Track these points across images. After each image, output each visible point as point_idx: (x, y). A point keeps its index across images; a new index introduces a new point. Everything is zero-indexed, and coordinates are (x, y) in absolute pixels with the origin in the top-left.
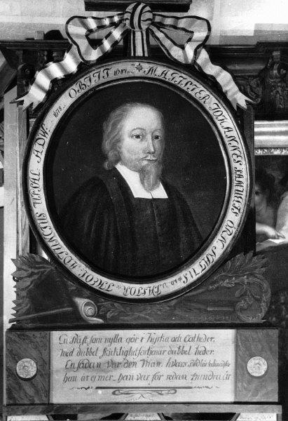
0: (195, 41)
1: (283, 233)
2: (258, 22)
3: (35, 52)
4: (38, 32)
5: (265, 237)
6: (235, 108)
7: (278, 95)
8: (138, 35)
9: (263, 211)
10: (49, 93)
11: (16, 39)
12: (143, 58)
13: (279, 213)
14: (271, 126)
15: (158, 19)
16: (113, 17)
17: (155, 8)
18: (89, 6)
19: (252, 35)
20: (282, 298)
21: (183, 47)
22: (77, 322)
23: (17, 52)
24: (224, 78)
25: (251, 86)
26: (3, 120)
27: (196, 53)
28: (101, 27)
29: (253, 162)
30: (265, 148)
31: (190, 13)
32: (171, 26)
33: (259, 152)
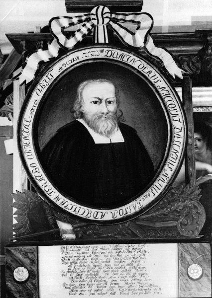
0: (144, 28)
5: (206, 172)
6: (174, 77)
10: (36, 74)
11: (21, 32)
12: (104, 45)
14: (208, 91)
17: (113, 10)
18: (70, 9)
19: (191, 25)
21: (133, 34)
22: (56, 239)
23: (22, 42)
25: (192, 62)
26: (13, 91)
27: (146, 41)
29: (191, 118)
30: (204, 107)
31: (142, 11)
33: (195, 110)
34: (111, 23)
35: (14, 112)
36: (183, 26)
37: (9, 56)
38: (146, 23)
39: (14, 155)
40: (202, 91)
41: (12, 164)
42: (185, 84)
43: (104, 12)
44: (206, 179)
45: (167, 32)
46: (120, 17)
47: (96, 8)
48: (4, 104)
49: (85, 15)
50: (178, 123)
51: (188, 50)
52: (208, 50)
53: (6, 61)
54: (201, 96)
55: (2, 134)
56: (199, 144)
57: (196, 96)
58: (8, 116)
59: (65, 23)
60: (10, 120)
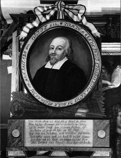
1: (114, 84)
4: (25, 11)
5: (107, 85)
7: (112, 34)
8: (61, 12)
10: (28, 34)
12: (62, 20)
13: (112, 77)
14: (109, 45)
15: (67, 6)
16: (49, 7)
17: (66, 3)
18: (42, 2)
19: (101, 12)
20: (113, 108)
24: (91, 26)
25: (102, 30)
28: (48, 9)
31: (78, 4)
35: (13, 53)
36: (97, 12)
37: (11, 25)
39: (12, 74)
42: (99, 41)
44: (107, 88)
45: (89, 15)
46: (70, 7)
48: (8, 49)
53: (9, 27)
54: (105, 47)
55: (6, 64)
57: (103, 47)
58: (9, 55)
60: (10, 56)
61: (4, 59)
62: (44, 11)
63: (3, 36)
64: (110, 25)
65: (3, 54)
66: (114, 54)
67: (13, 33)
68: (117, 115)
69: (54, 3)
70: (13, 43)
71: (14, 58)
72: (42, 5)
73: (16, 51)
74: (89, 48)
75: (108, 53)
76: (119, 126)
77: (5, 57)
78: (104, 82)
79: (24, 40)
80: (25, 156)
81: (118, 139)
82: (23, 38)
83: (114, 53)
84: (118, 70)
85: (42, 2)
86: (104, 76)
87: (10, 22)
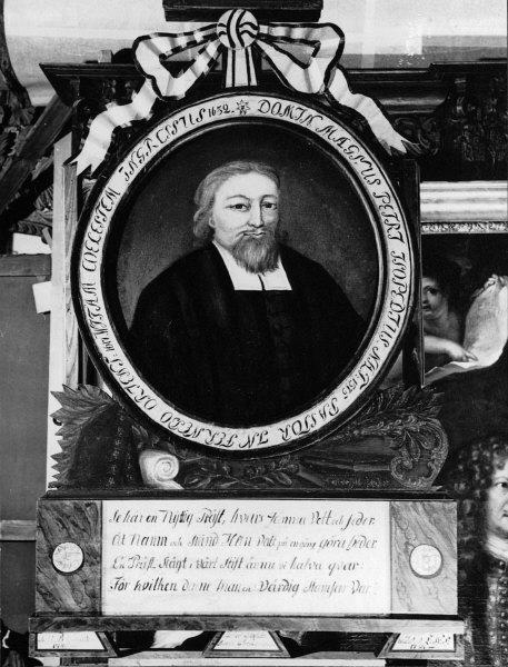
1: (474, 352)
2: (430, 33)
3: (100, 81)
5: (446, 358)
8: (240, 53)
9: (445, 317)
10: (112, 149)
11: (72, 62)
12: (247, 90)
13: (468, 321)
20: (474, 453)
21: (305, 66)
22: (139, 488)
24: (367, 107)
27: (328, 78)
31: (321, 21)
32: (283, 38)
34: (260, 43)
37: (46, 110)
38: (329, 43)
39: (52, 315)
40: (441, 190)
41: (48, 333)
42: (405, 175)
43: (242, 22)
44: (447, 371)
47: (229, 13)
48: (35, 209)
49: (202, 29)
50: (399, 248)
51: (412, 106)
52: (455, 105)
53: (40, 119)
55: (29, 271)
56: (432, 299)
57: (429, 201)
58: (41, 235)
59: (164, 46)
60: (44, 241)
61: (20, 253)
62: (177, 50)
63: (14, 155)
64: (459, 108)
65: (17, 232)
66: (475, 230)
67: (56, 145)
68: (489, 484)
69: (216, 15)
70: (55, 185)
71: (59, 250)
72: (174, 27)
73: (67, 219)
74: (360, 201)
75: (448, 223)
76: (499, 529)
77: (24, 244)
78: (431, 343)
79: (95, 175)
80: (101, 651)
81: (495, 580)
82: (90, 166)
83: (476, 223)
84: (491, 295)
85: (170, 16)
86: (433, 321)
87: (43, 97)
